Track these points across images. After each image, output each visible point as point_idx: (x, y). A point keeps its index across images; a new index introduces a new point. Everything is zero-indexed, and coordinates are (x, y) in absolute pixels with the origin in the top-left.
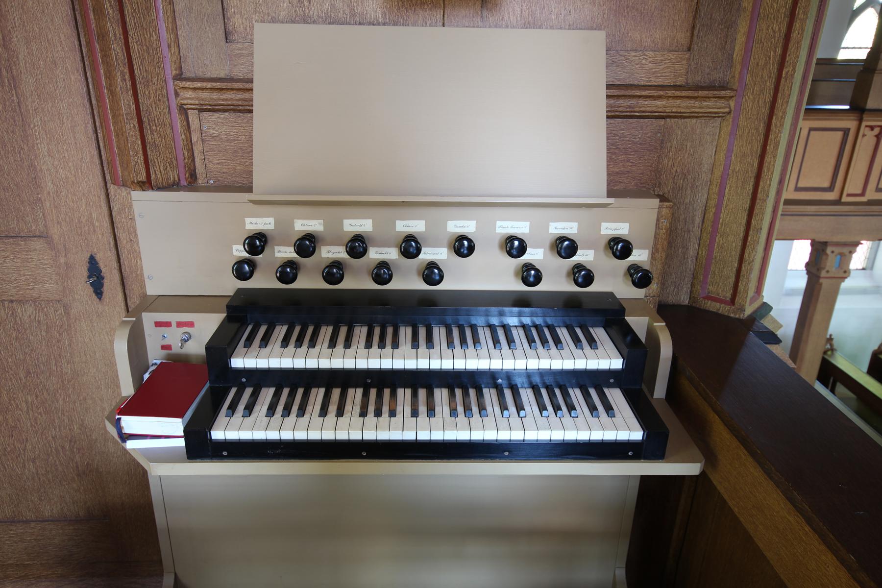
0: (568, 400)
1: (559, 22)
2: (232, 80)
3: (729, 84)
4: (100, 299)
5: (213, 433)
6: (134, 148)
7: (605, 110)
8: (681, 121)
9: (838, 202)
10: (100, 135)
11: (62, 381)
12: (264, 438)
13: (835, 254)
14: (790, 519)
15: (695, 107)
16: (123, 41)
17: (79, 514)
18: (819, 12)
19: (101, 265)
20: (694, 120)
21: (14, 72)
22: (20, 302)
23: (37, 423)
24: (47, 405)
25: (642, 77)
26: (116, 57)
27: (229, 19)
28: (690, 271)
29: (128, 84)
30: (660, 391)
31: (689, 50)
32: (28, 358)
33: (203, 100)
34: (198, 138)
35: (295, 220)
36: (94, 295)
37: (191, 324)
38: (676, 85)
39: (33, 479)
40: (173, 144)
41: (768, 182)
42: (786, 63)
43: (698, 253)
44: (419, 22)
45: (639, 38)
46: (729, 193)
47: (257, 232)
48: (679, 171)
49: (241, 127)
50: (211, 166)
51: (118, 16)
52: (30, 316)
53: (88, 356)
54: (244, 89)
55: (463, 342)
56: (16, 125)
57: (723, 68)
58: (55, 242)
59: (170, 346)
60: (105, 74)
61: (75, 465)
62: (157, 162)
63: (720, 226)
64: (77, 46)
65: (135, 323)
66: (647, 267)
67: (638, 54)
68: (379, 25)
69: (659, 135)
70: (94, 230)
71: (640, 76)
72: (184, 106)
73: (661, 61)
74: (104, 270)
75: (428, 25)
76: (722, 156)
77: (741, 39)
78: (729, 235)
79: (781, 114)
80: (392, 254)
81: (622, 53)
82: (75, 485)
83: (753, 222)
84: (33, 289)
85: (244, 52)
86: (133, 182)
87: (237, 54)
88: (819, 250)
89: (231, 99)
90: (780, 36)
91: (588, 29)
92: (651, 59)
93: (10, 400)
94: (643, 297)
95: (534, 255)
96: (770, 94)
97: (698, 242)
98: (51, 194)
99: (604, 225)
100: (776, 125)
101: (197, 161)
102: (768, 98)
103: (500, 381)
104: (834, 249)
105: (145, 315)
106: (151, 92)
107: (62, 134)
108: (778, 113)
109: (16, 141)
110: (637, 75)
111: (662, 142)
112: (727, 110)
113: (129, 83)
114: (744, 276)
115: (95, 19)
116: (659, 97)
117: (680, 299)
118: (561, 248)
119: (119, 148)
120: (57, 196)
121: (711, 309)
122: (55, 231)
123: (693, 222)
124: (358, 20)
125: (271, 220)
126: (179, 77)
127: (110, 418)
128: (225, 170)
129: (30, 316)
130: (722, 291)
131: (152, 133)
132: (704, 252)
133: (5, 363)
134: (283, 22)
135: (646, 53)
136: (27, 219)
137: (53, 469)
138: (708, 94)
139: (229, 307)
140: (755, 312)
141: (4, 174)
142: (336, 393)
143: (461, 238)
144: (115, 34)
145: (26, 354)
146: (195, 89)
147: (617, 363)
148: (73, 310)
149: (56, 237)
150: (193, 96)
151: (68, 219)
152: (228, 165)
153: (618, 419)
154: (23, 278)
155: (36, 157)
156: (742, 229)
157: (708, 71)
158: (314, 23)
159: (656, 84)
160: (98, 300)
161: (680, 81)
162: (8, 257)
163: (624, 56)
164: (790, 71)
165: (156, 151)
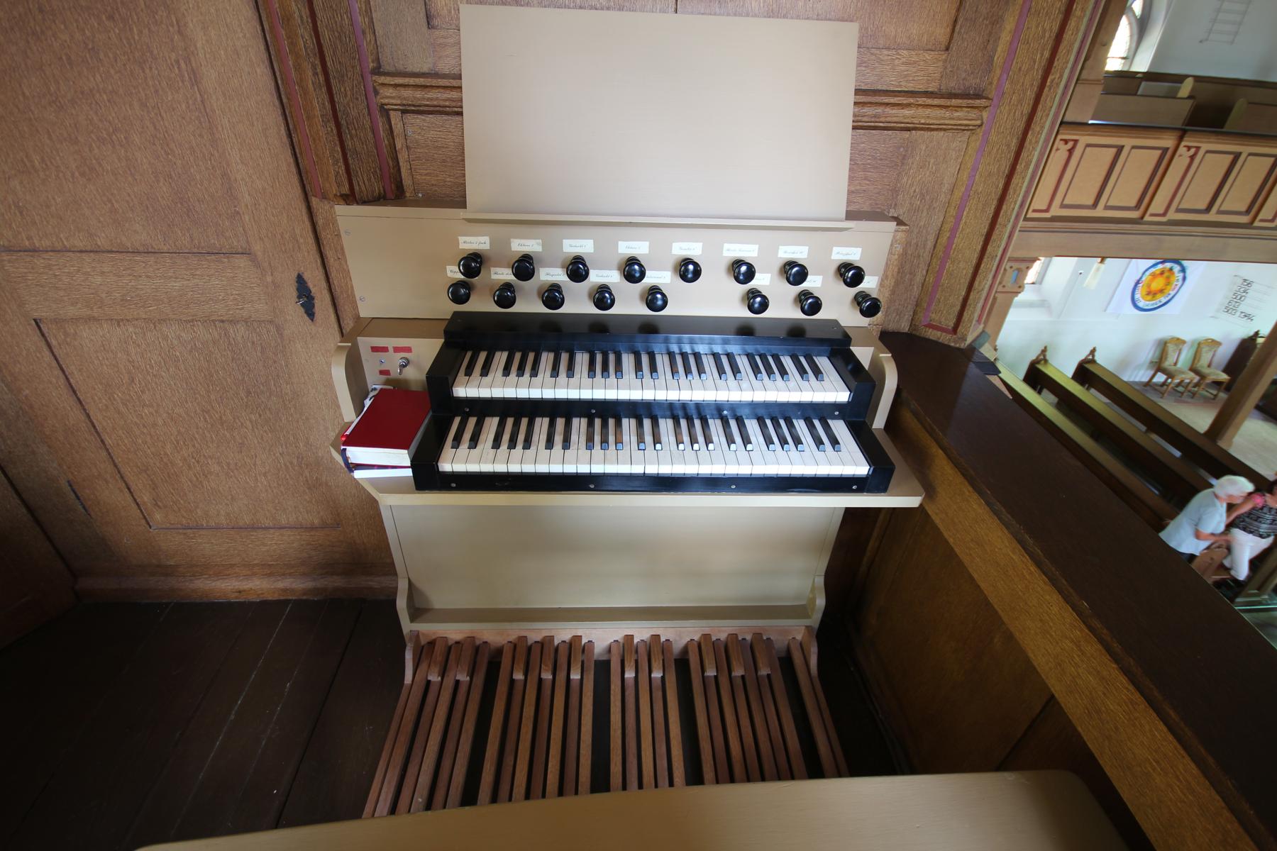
0: (793, 431)
1: (806, 11)
2: (437, 75)
3: (985, 92)
4: (312, 320)
6: (334, 156)
7: (851, 119)
11: (283, 401)
12: (492, 470)
13: (1012, 269)
14: (1014, 557)
15: (945, 118)
16: (311, 25)
18: (954, 26)
19: (310, 285)
20: (941, 133)
21: (194, 65)
22: (233, 322)
23: (263, 440)
25: (892, 81)
26: (305, 46)
28: (915, 298)
29: (321, 79)
30: (879, 422)
31: (947, 49)
32: (246, 379)
33: (405, 99)
34: (402, 145)
35: (512, 240)
36: (305, 315)
37: (408, 350)
38: (927, 92)
39: (267, 491)
41: (1012, 206)
42: (1053, 68)
43: (925, 280)
44: (649, 7)
46: (967, 216)
47: (471, 252)
48: (917, 190)
49: (450, 132)
52: (243, 337)
54: (450, 87)
56: (203, 128)
57: (981, 72)
58: (259, 259)
59: (387, 348)
60: (294, 66)
62: (359, 173)
63: (952, 251)
64: (259, 32)
65: (350, 348)
66: (874, 295)
68: (602, 9)
70: (299, 248)
71: (890, 82)
72: (385, 107)
73: (915, 62)
74: (313, 290)
75: (658, 11)
76: (965, 175)
77: (1005, 37)
78: (960, 262)
80: (612, 277)
81: (873, 51)
83: (989, 248)
84: (242, 309)
86: (335, 195)
87: (440, 44)
90: (1050, 37)
91: (838, 20)
92: (904, 59)
93: (234, 418)
95: (761, 281)
96: (1029, 104)
97: (927, 268)
98: (249, 207)
99: (836, 249)
100: (1031, 140)
102: (1026, 109)
103: (725, 412)
105: (360, 339)
106: (348, 88)
107: (254, 138)
108: (1035, 127)
109: (205, 145)
110: (887, 79)
111: (904, 157)
112: (979, 122)
113: (322, 78)
114: (970, 305)
116: (908, 105)
117: (901, 326)
118: (790, 275)
121: (931, 338)
122: (257, 248)
123: (924, 248)
126: (378, 71)
127: (337, 449)
129: (243, 337)
130: (945, 319)
131: (352, 138)
132: (932, 279)
136: (227, 234)
138: (961, 103)
139: (446, 332)
140: (974, 341)
141: (196, 184)
142: (560, 422)
143: (687, 261)
144: (301, 17)
145: (244, 374)
146: (396, 86)
147: (843, 396)
149: (259, 254)
150: (394, 95)
151: (270, 235)
154: (231, 298)
155: (228, 165)
157: (964, 75)
158: (527, 6)
159: (906, 89)
162: (212, 275)
163: (875, 55)
164: (1057, 79)
165: (358, 160)
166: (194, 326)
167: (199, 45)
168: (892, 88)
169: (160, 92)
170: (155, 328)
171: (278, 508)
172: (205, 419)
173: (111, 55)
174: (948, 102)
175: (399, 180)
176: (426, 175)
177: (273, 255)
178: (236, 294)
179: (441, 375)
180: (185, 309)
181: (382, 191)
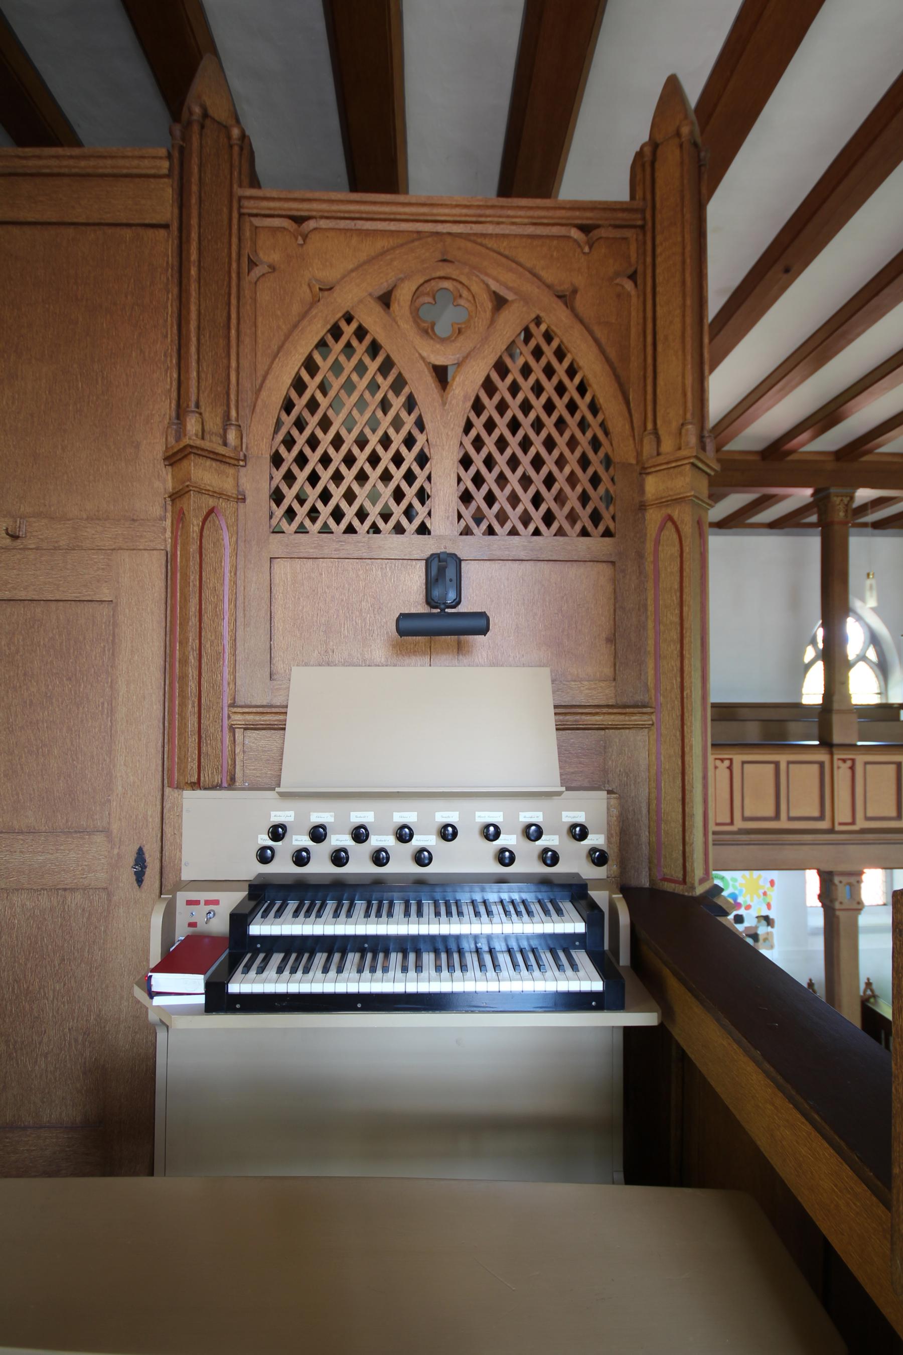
2: (271, 706)
4: (140, 886)
5: (230, 985)
8: (617, 732)
9: (831, 831)
10: (166, 749)
11: (91, 969)
15: (625, 721)
17: (76, 1120)
19: (147, 856)
20: (627, 731)
22: (72, 890)
23: (58, 1013)
24: (72, 993)
27: (274, 665)
31: (614, 680)
32: (66, 945)
35: (311, 813)
36: (135, 882)
37: (216, 902)
40: (221, 754)
41: (691, 777)
45: (576, 673)
48: (622, 770)
50: (248, 772)
51: (197, 664)
53: (119, 942)
55: (449, 913)
61: (83, 1060)
66: (605, 849)
67: (576, 683)
68: (383, 666)
69: (602, 742)
70: (147, 825)
71: (581, 699)
73: (594, 688)
74: (148, 860)
76: (654, 758)
79: (689, 724)
80: (389, 841)
81: (564, 683)
82: (78, 1085)
84: (86, 877)
85: (282, 686)
86: (187, 783)
88: (827, 880)
89: (270, 720)
93: (40, 988)
94: (605, 877)
97: (647, 830)
101: (238, 767)
102: (679, 713)
104: (841, 878)
109: (102, 754)
111: (605, 747)
112: (650, 722)
113: (196, 709)
115: (179, 667)
116: (597, 714)
117: (641, 882)
119: (179, 758)
120: (123, 797)
122: (115, 827)
124: (368, 663)
125: (292, 813)
128: (258, 775)
131: (207, 746)
133: (45, 950)
134: (313, 666)
135: (583, 682)
136: (95, 817)
137: (62, 1065)
144: (193, 676)
145: (65, 940)
146: (244, 713)
147: (580, 927)
148: (115, 897)
152: (261, 770)
153: (581, 973)
155: (114, 767)
156: (680, 817)
160: (138, 887)
161: (611, 702)
166: (40, 894)
167: (121, 694)
168: (583, 704)
169: (85, 721)
170: (7, 898)
171: (45, 1100)
172: (13, 989)
173: (60, 700)
174: (624, 711)
175: (233, 773)
176: (254, 770)
177: (125, 832)
178: (85, 865)
179: (239, 920)
180: (40, 879)
181: (220, 782)
